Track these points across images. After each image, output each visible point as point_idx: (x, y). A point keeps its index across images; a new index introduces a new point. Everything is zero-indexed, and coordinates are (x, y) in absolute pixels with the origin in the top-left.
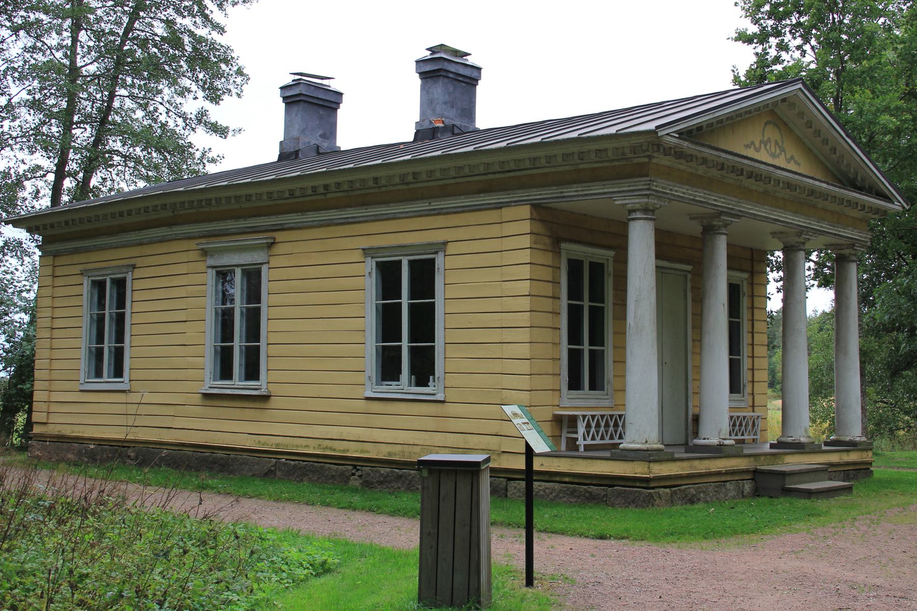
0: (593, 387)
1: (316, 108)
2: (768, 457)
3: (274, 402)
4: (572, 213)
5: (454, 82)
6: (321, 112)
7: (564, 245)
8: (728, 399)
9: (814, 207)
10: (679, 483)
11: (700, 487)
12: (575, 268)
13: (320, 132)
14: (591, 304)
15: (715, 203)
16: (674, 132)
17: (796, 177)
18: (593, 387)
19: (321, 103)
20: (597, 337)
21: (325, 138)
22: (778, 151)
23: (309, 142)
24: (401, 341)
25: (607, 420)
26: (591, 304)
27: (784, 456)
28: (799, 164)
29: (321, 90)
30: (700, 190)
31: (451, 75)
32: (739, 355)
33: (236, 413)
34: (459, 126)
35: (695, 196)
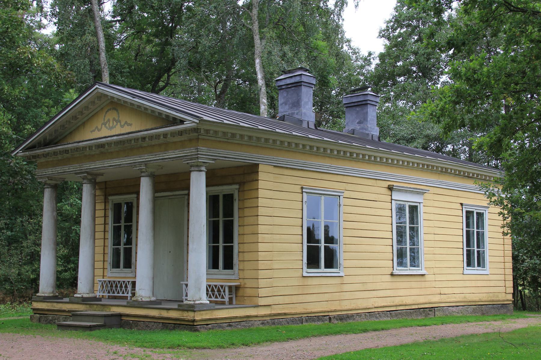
0: (479, 265)
1: (354, 108)
2: (99, 306)
3: (427, 278)
4: (117, 180)
5: (287, 90)
6: (358, 109)
7: (110, 198)
8: (205, 273)
9: (141, 147)
10: (46, 313)
11: (54, 317)
12: (117, 207)
13: (357, 121)
14: (114, 225)
15: (69, 170)
16: (20, 151)
17: (121, 137)
18: (479, 265)
19: (356, 104)
20: (229, 237)
21: (360, 124)
22: (115, 123)
23: (348, 130)
24: (219, 243)
25: (107, 284)
26: (114, 225)
27: (110, 307)
28: (131, 125)
29: (354, 97)
30: (57, 167)
31: (283, 87)
32: (113, 248)
33: (414, 285)
34: (288, 114)
35: (58, 171)
